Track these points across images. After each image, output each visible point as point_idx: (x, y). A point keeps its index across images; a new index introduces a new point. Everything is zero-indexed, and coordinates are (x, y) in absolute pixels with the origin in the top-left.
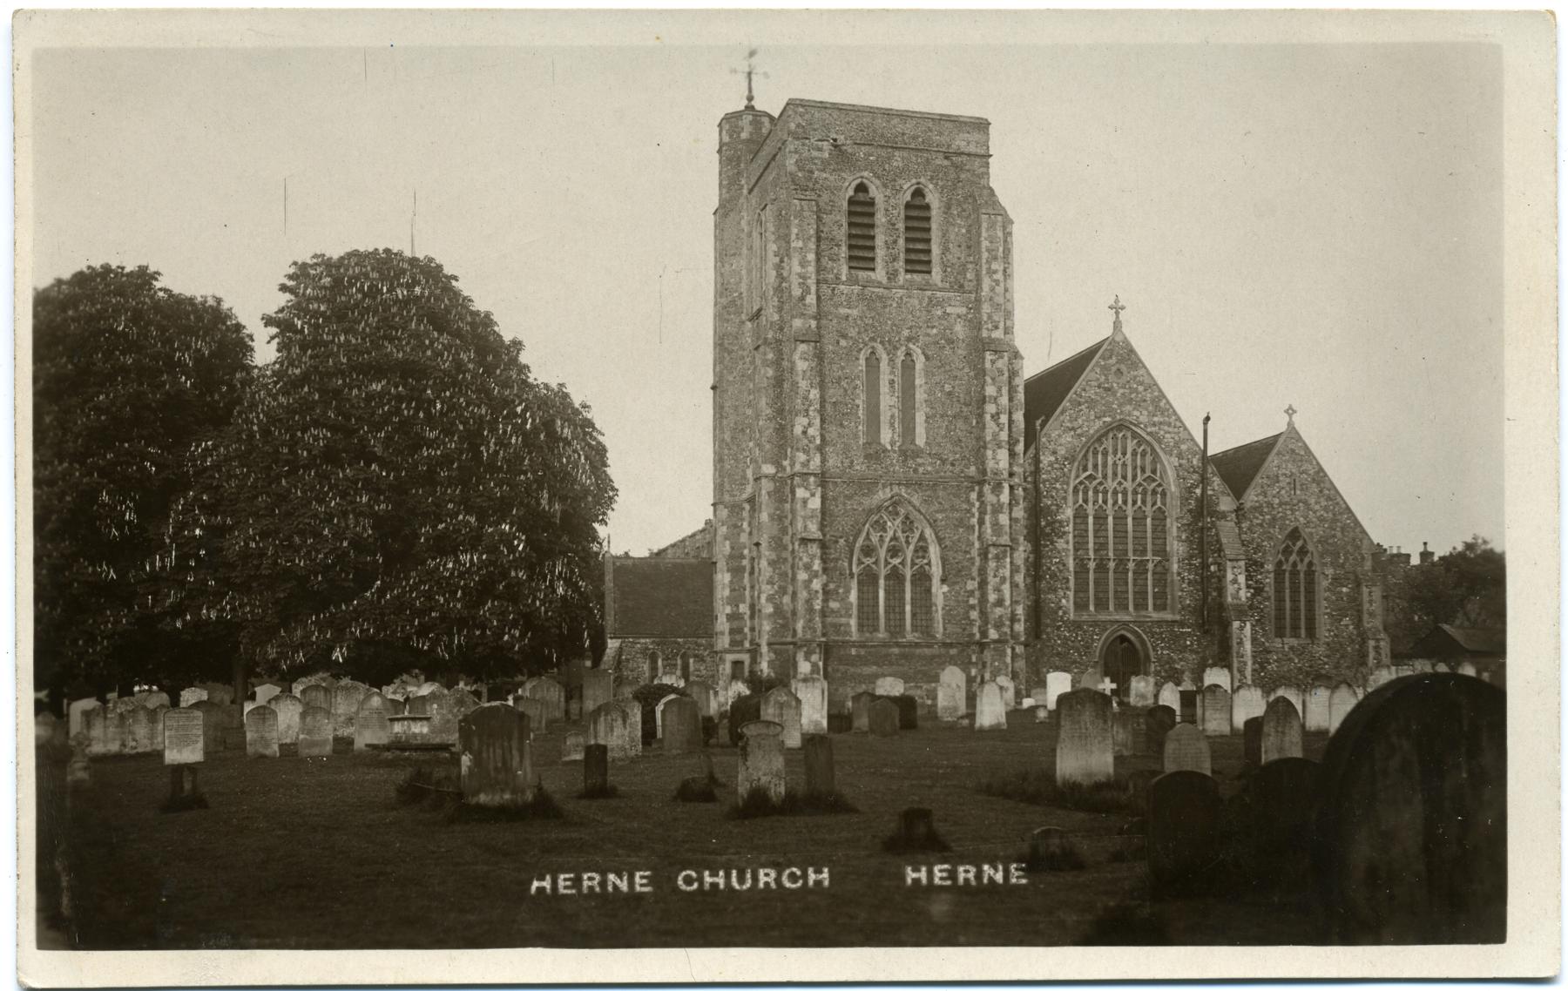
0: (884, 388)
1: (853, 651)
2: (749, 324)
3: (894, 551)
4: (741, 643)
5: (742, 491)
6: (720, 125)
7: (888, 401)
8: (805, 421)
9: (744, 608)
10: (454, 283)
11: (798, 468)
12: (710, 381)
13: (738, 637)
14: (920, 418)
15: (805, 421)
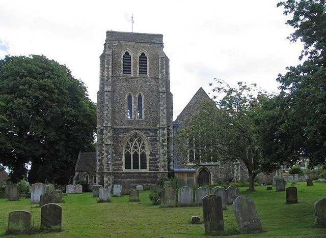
0: (133, 104)
8: (107, 112)
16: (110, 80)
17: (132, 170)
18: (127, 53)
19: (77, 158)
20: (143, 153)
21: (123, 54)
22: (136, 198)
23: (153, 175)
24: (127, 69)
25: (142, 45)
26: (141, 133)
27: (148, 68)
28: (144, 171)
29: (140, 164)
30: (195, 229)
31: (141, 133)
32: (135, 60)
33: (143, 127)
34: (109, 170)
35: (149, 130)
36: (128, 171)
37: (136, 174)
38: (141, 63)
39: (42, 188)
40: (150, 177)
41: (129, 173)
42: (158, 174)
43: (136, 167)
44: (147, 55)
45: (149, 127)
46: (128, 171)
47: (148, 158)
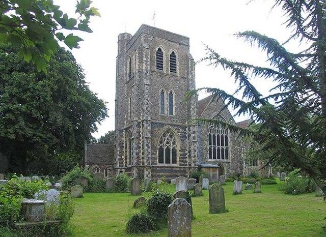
0: (165, 100)
1: (308, 142)
2: (126, 85)
3: (167, 143)
4: (123, 166)
5: (123, 127)
6: (119, 36)
7: (167, 103)
8: (147, 106)
9: (123, 157)
10: (97, 11)
11: (145, 118)
12: (115, 99)
13: (122, 165)
14: (174, 109)
15: (147, 106)
16: (148, 74)
17: (165, 164)
18: (160, 50)
19: (83, 149)
20: (174, 148)
21: (157, 50)
22: (259, 189)
23: (182, 169)
24: (160, 66)
25: (172, 43)
26: (173, 129)
27: (177, 67)
28: (175, 165)
29: (171, 158)
30: (297, 212)
31: (173, 129)
32: (167, 58)
33: (175, 123)
34: (149, 163)
35: (180, 126)
36: (161, 165)
37: (169, 169)
38: (172, 59)
39: (184, 181)
40: (180, 171)
41: (163, 167)
42: (186, 169)
43: (168, 162)
44: (176, 54)
45: (180, 124)
46: (161, 165)
47: (178, 153)
